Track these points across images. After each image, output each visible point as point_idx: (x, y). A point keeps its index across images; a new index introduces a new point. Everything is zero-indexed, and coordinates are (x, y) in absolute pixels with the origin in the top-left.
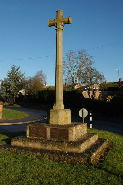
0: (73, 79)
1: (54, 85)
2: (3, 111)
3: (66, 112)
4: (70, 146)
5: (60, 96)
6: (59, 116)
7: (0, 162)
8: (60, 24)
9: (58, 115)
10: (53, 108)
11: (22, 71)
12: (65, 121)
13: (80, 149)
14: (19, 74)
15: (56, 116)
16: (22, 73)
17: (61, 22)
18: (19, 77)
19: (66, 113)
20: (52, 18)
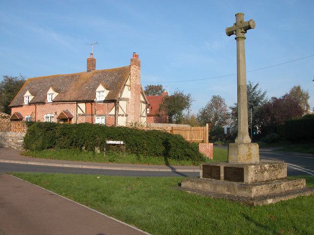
0: (115, 115)
1: (153, 117)
2: (214, 152)
3: (250, 146)
4: (241, 188)
5: (244, 127)
6: (239, 152)
7: (1, 102)
8: (240, 31)
9: (238, 151)
10: (234, 142)
11: (261, 89)
12: (248, 159)
13: (251, 192)
14: (257, 95)
15: (236, 152)
16: (262, 94)
17: (241, 29)
18: (258, 100)
19: (249, 148)
20: (231, 23)
